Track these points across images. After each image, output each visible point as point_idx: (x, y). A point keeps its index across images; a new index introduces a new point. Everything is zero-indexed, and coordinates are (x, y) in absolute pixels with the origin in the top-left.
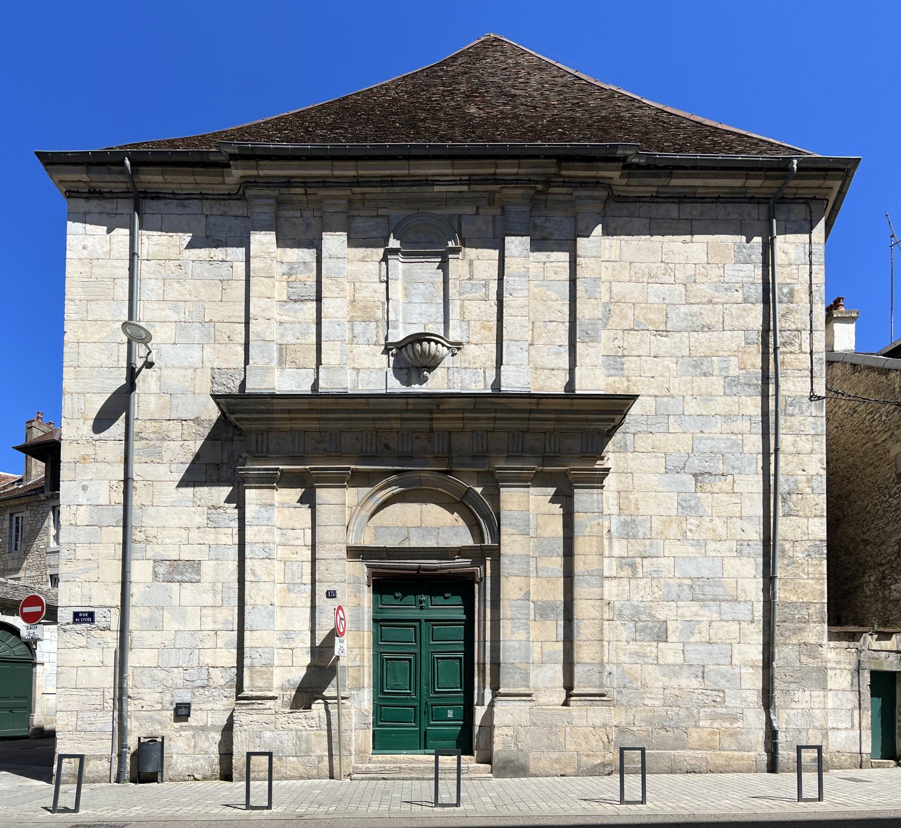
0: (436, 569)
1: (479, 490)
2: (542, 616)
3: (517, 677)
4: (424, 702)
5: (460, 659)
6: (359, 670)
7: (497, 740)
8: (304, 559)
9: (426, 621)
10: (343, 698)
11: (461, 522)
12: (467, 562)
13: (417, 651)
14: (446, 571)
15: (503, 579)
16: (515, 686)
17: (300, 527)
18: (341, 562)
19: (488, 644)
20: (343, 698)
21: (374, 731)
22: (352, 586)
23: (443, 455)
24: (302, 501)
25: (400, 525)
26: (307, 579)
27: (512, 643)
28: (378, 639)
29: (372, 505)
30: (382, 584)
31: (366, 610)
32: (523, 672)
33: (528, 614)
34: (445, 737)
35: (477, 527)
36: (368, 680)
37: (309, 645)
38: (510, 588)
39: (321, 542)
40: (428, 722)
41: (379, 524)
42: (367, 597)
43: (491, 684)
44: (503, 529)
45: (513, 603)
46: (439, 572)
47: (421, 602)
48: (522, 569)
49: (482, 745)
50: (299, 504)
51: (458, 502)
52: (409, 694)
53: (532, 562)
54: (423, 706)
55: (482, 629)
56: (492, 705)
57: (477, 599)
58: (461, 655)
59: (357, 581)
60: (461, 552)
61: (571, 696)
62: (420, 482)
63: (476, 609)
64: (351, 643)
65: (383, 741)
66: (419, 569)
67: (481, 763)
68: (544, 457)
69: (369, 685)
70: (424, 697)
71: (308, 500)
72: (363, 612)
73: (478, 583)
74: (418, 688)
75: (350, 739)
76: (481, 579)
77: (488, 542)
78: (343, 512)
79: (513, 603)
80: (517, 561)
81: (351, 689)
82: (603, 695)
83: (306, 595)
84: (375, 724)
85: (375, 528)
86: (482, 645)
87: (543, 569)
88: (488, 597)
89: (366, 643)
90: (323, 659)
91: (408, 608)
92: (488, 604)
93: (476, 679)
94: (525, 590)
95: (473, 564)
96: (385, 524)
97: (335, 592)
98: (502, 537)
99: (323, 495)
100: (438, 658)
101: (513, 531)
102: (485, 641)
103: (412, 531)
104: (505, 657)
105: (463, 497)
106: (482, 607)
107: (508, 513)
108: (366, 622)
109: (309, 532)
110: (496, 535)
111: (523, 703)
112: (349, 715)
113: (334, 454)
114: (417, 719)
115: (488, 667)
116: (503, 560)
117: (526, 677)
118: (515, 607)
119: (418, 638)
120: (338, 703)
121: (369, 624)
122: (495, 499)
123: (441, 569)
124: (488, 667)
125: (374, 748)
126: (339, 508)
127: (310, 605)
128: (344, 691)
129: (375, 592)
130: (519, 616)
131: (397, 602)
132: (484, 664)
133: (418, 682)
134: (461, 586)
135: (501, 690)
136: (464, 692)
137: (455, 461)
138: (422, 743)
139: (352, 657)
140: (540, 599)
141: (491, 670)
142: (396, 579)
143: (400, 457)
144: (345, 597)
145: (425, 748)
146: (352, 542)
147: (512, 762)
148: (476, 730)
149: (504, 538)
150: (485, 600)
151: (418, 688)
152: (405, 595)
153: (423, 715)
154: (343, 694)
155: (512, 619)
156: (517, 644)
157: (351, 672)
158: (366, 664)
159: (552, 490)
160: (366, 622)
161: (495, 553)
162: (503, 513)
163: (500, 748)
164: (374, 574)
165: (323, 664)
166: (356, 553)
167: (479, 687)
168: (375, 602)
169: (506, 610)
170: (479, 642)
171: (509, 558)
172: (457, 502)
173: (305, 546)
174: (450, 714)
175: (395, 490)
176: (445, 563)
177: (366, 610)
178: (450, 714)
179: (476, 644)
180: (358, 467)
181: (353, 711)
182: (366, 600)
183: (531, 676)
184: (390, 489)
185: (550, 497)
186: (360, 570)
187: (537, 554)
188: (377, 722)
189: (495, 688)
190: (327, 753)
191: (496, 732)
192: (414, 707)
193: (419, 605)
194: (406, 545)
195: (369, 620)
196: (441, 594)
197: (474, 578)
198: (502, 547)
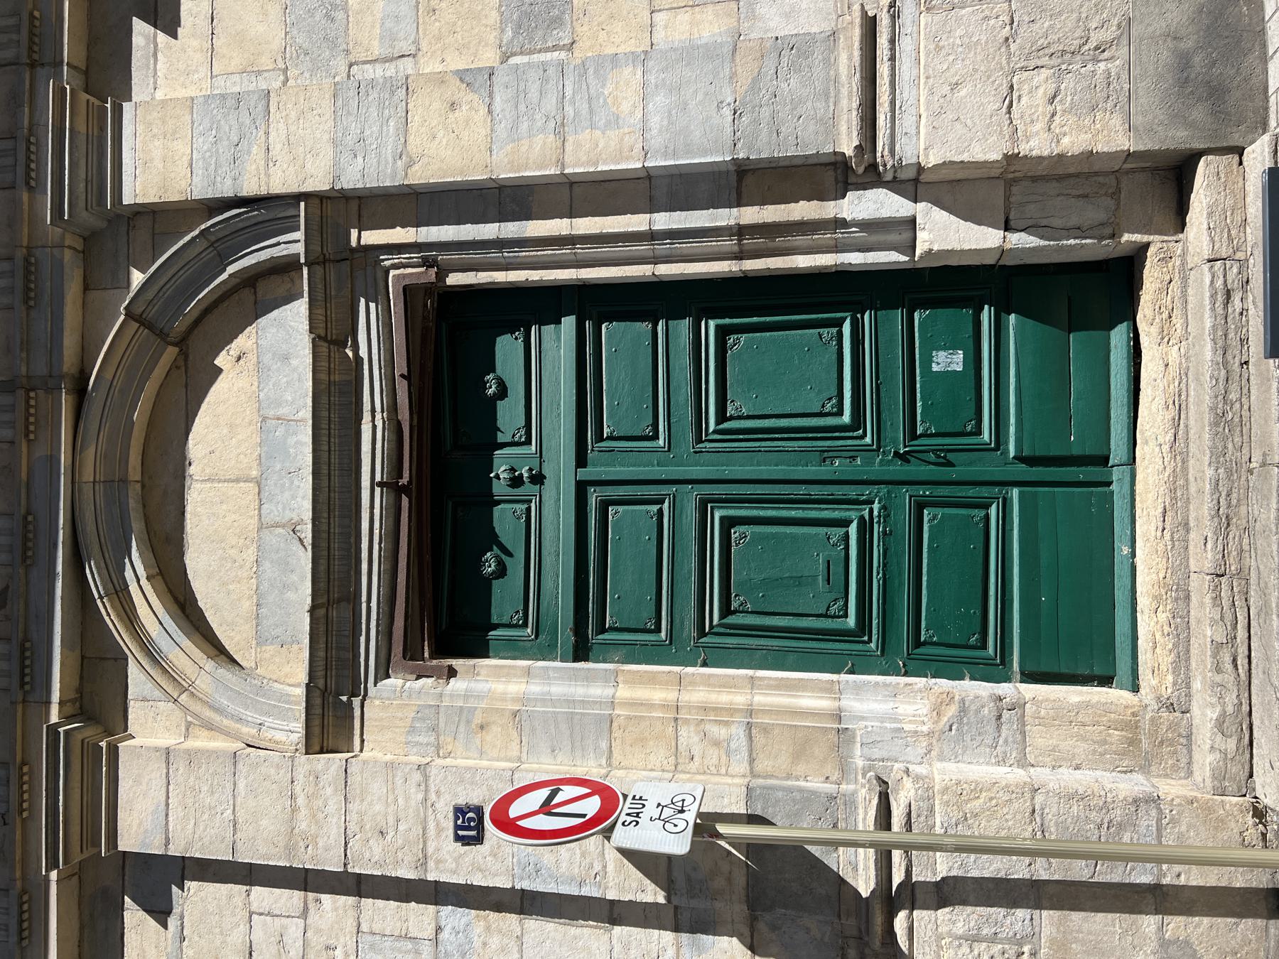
0: (395, 426)
1: (137, 278)
2: (557, 22)
3: (791, 85)
4: (898, 469)
5: (723, 333)
6: (765, 729)
7: (1073, 142)
8: (350, 924)
9: (581, 461)
10: (884, 819)
11: (243, 342)
12: (368, 316)
13: (690, 497)
14: (402, 388)
15: (420, 176)
16: (829, 92)
17: (243, 928)
18: (354, 779)
19: (663, 221)
20: (884, 819)
21: (1031, 677)
22: (446, 739)
23: (21, 406)
24: (161, 911)
25: (251, 554)
26: (419, 917)
27: (655, 122)
28: (655, 642)
29: (181, 652)
30: (451, 616)
31: (535, 688)
32: (770, 65)
33: (544, 67)
34: (1051, 382)
35: (262, 286)
36: (802, 694)
37: (668, 936)
38: (449, 147)
39: (290, 850)
40: (984, 449)
41: (247, 630)
42: (490, 681)
43: (822, 198)
44: (250, 188)
45: (502, 130)
46: (404, 415)
47: (516, 482)
48: (381, 106)
49: (1093, 214)
50: (172, 922)
51: (184, 354)
52: (865, 528)
53: (370, 72)
54: (916, 469)
55: (605, 250)
56: (914, 183)
57: (500, 277)
58: (710, 327)
59: (431, 721)
60: (331, 337)
61: (873, 166)
62: (115, 484)
63: (535, 276)
64: (660, 756)
65: (1078, 638)
66: (392, 486)
67: (1182, 209)
68: (33, 65)
69: (829, 689)
70: (877, 467)
71: (159, 879)
72: (545, 700)
73: (441, 275)
74: (839, 491)
75: (1072, 796)
76: (427, 263)
77: (293, 244)
78: (192, 757)
79: (502, 130)
80: (355, 129)
81: (845, 769)
82: (870, 25)
83: (479, 928)
84: (995, 671)
85: (261, 641)
86: (663, 247)
87: (389, 37)
88: (489, 231)
89: (659, 695)
90: (719, 883)
91: (538, 521)
92: (511, 229)
93: (803, 262)
94: (455, 89)
95: (378, 293)
96: (247, 605)
97: (459, 811)
98: (277, 187)
99: (138, 829)
100: (722, 416)
101: (257, 151)
102: (651, 236)
103: (273, 512)
104: (708, 147)
105: (162, 335)
106: (524, 254)
107: (199, 171)
108: (579, 691)
109: (262, 896)
110: (268, 211)
111: (905, 45)
112: (960, 792)
113: (14, 788)
114: (973, 496)
115: (751, 215)
116: (351, 179)
117: (793, 50)
118: (515, 126)
119: (642, 491)
120: (907, 849)
121: (589, 678)
122: (160, 219)
123: (393, 408)
124: (751, 215)
125: (1106, 681)
126: (180, 767)
127: (511, 920)
128: (850, 802)
129: (480, 650)
130: (550, 103)
131: (515, 567)
132: (741, 231)
133: (815, 491)
134: (457, 334)
135: (847, 144)
136: (857, 308)
137: (40, 368)
138: (1081, 473)
139: (713, 755)
140: (492, 37)
141: (763, 202)
142: (433, 571)
143: (25, 558)
144: (481, 773)
145: (1105, 460)
146: (292, 729)
147: (1183, 62)
148: (1020, 240)
149: (281, 181)
150: (500, 244)
151: (839, 491)
152: (492, 539)
153: (953, 474)
154: (866, 818)
155: (560, 131)
156: (660, 101)
157: (774, 762)
158: (740, 699)
159: (140, 28)
160: (579, 691)
161: (335, 210)
162: (201, 190)
163: (1116, 121)
164: (411, 653)
165: (740, 880)
166: (330, 717)
167: (837, 248)
168: (515, 650)
169: (526, 158)
170: (656, 261)
171: (345, 157)
172: (185, 352)
173: (305, 913)
174: (949, 361)
175: (136, 569)
176: (373, 395)
177: (535, 688)
178: (949, 361)
179: (666, 270)
180: (56, 696)
181: (944, 772)
182: (499, 687)
183: (786, 30)
184: (133, 588)
185: (162, 37)
186: (395, 703)
187: (341, 65)
188: (989, 662)
189: (837, 175)
190: (1149, 923)
191: (1036, 144)
192: (920, 507)
193: (528, 488)
194: (307, 532)
195: (574, 677)
196: (489, 408)
197: (428, 289)
198: (309, 187)
